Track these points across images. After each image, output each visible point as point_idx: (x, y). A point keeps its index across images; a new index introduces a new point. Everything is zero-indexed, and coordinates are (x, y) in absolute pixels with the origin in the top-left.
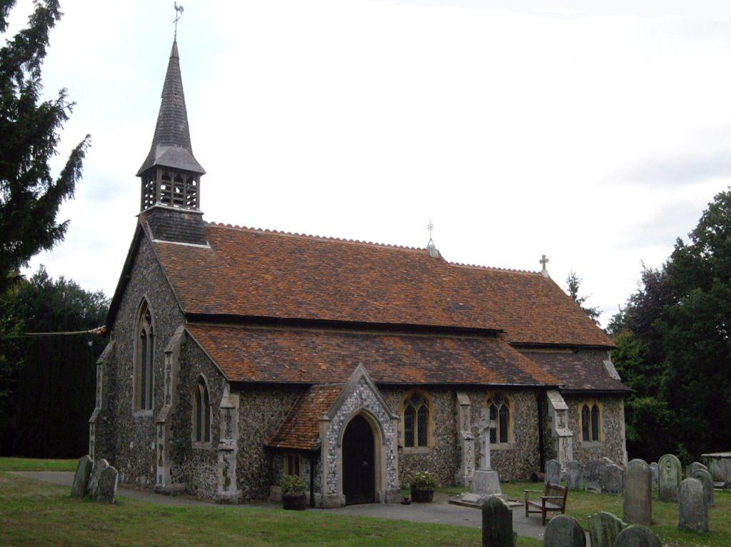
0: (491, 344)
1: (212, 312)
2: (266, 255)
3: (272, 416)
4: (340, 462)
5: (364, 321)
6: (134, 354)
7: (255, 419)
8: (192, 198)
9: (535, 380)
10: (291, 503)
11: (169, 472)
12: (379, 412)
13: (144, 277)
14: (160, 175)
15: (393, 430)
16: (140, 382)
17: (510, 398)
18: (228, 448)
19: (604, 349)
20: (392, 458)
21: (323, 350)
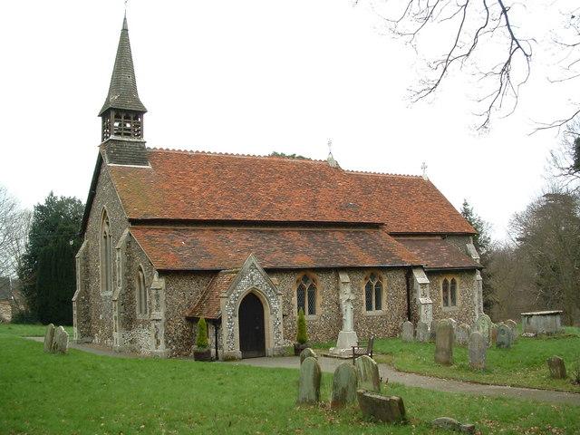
8: (138, 131)
14: (113, 114)
16: (104, 270)
21: (235, 243)
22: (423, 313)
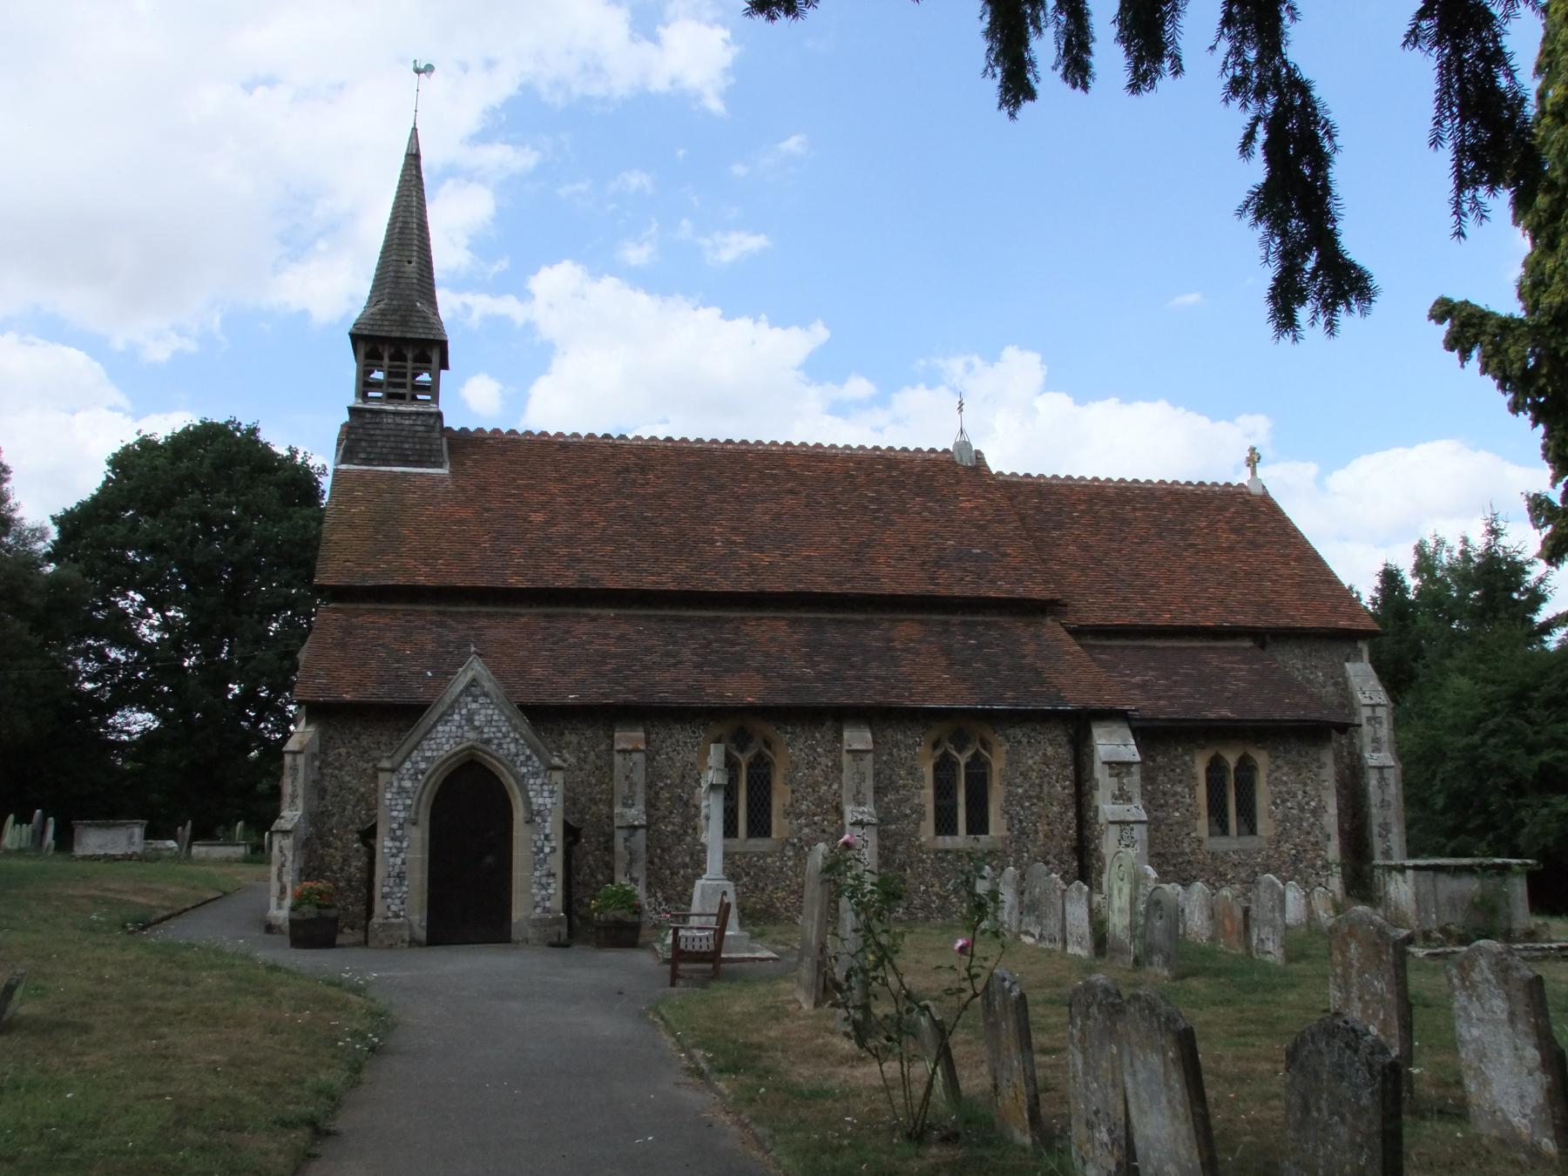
12: (517, 755)
15: (552, 792)
20: (547, 850)
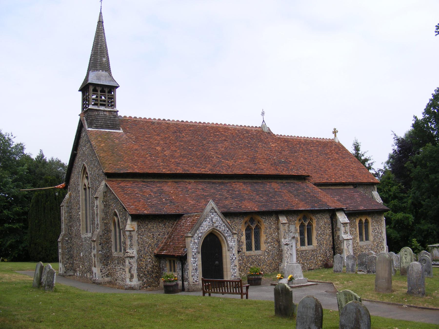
0: (302, 185)
1: (122, 172)
2: (158, 135)
3: (159, 235)
4: (200, 263)
5: (220, 173)
6: (80, 199)
7: (149, 237)
9: (328, 205)
10: (170, 289)
11: (100, 270)
12: (225, 230)
13: (84, 152)
14: (91, 88)
15: (234, 241)
17: (313, 218)
18: (131, 256)
19: (372, 184)
20: (234, 258)
22: (345, 247)
